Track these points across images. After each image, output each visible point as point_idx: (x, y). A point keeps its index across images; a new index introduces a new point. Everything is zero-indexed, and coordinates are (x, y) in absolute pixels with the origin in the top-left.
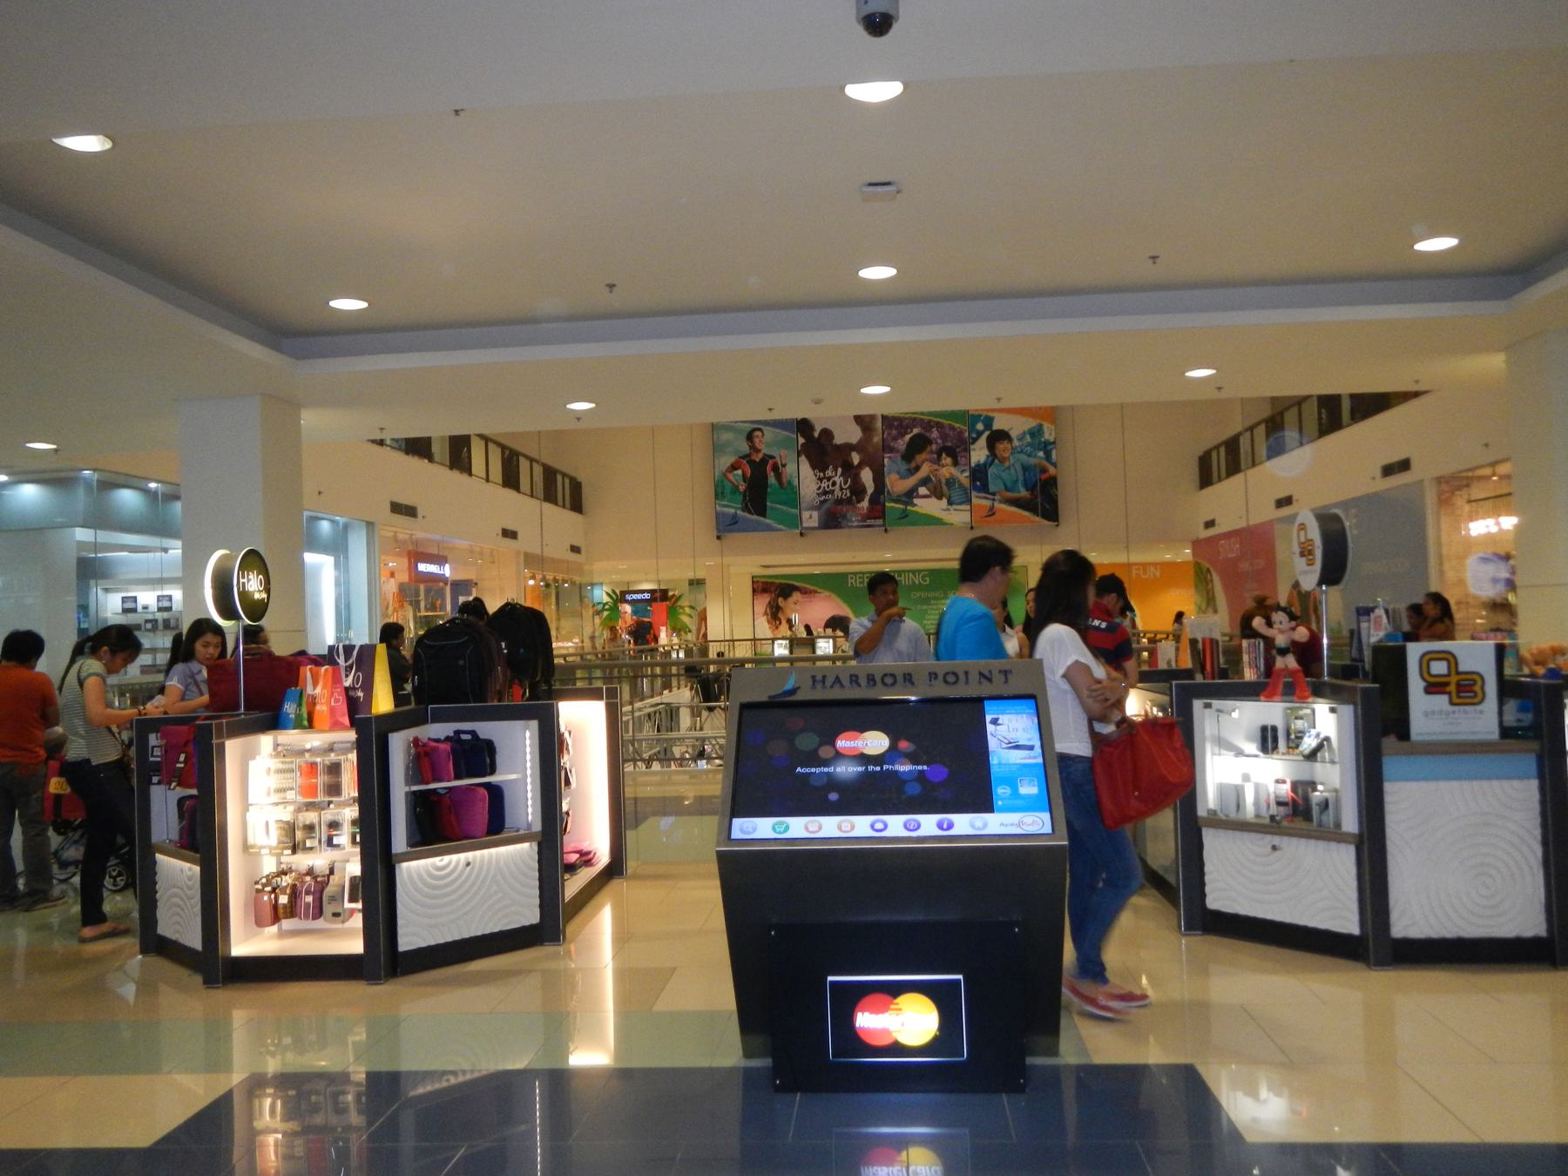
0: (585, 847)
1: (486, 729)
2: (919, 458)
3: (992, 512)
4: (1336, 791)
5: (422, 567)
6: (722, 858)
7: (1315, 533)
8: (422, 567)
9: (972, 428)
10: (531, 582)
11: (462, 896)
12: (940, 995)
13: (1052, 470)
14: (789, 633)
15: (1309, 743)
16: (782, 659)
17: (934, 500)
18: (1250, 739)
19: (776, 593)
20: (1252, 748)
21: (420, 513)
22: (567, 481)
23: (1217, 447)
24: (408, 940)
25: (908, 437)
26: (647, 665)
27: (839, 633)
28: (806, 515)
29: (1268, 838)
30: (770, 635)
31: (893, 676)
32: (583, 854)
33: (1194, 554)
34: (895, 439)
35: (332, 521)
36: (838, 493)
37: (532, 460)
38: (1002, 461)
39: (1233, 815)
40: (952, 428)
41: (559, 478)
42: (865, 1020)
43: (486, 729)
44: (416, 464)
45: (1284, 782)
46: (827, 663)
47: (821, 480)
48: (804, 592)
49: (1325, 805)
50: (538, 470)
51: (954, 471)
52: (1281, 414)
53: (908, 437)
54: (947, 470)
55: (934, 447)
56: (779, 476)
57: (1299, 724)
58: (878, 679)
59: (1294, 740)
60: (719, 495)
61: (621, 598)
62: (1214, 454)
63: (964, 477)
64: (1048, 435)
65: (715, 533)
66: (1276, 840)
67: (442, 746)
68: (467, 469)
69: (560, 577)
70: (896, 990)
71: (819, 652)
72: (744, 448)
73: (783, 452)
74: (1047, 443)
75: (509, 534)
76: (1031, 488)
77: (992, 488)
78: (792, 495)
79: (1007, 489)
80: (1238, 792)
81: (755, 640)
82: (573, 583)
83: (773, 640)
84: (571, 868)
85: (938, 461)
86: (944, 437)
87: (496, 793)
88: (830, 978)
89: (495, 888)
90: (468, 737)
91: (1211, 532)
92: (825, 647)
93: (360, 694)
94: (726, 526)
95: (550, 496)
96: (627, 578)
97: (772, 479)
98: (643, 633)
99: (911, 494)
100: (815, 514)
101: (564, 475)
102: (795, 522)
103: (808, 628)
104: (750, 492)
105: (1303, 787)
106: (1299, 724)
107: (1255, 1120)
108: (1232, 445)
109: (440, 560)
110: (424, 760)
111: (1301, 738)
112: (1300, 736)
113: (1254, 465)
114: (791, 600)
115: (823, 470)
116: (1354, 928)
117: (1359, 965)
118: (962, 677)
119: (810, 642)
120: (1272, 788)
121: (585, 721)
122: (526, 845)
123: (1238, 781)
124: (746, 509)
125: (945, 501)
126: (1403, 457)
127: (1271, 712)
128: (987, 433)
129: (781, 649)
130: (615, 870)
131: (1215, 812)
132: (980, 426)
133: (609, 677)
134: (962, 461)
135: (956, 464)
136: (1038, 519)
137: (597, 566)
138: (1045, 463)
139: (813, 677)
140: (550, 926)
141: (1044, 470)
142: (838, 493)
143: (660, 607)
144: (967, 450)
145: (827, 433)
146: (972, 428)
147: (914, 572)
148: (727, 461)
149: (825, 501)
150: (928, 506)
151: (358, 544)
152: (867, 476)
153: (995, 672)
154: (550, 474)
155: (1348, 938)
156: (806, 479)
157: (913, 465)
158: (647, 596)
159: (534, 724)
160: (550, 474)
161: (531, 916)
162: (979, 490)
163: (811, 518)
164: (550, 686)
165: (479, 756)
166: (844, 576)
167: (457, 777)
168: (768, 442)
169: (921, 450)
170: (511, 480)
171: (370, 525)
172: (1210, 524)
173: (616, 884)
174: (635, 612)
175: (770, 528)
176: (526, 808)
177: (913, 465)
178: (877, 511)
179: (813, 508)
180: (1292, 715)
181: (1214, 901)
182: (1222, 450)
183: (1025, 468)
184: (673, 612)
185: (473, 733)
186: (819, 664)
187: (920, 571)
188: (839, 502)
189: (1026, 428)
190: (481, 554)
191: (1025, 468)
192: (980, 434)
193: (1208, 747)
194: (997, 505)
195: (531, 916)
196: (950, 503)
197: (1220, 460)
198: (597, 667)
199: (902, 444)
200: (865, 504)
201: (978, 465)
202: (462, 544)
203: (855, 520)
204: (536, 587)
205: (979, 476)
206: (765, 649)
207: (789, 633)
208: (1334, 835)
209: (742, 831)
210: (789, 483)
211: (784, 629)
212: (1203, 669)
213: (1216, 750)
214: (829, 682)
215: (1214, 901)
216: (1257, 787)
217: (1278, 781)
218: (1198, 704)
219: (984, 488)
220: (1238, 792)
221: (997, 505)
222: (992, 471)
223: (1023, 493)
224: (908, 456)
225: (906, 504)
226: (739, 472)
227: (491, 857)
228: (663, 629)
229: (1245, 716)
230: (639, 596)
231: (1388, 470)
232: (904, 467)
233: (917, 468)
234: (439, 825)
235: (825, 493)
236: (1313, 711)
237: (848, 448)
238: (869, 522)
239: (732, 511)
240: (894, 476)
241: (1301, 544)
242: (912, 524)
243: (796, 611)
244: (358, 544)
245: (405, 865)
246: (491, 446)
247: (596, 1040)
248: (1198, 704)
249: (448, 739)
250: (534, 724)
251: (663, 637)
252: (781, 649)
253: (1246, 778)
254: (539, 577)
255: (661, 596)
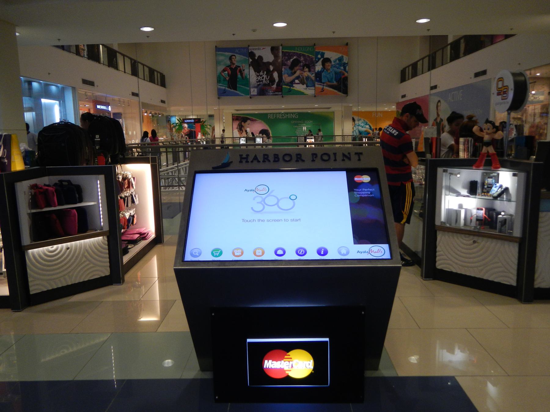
0: (143, 230)
1: (76, 179)
2: (296, 68)
3: (323, 90)
4: (511, 215)
5: (98, 107)
6: (178, 272)
7: (510, 82)
8: (98, 107)
9: (316, 57)
10: (146, 114)
11: (65, 264)
12: (311, 349)
13: (346, 74)
14: (246, 136)
15: (495, 191)
16: (243, 145)
17: (301, 85)
18: (464, 187)
19: (241, 120)
20: (465, 192)
21: (81, 81)
22: (159, 74)
23: (409, 66)
24: (35, 288)
25: (292, 60)
26: (190, 146)
27: (264, 136)
28: (252, 90)
29: (471, 237)
30: (239, 136)
31: (290, 155)
32: (141, 234)
33: (397, 108)
34: (287, 60)
35: (57, 86)
36: (264, 81)
37: (144, 65)
38: (327, 71)
39: (453, 225)
40: (309, 57)
41: (156, 73)
42: (269, 364)
43: (76, 179)
44: (65, 53)
45: (482, 209)
46: (260, 147)
47: (258, 76)
48: (252, 120)
49: (504, 222)
50: (147, 70)
51: (309, 74)
52: (435, 53)
53: (292, 60)
54: (306, 73)
55: (302, 64)
56: (242, 74)
57: (490, 181)
58: (281, 157)
59: (486, 189)
60: (219, 81)
61: (183, 121)
62: (407, 69)
63: (313, 76)
64: (345, 60)
65: (217, 96)
66: (476, 238)
67: (50, 188)
68: (116, 67)
69: (157, 112)
70: (288, 347)
71: (257, 142)
72: (228, 63)
73: (244, 65)
74: (345, 64)
75: (135, 94)
76: (338, 80)
77: (323, 81)
78: (246, 82)
79: (329, 81)
80: (458, 213)
81: (233, 138)
82: (163, 115)
83: (240, 138)
84: (134, 242)
85: (303, 70)
86: (305, 60)
87: (83, 213)
88: (249, 340)
89: (84, 259)
90: (66, 183)
91: (404, 99)
92: (259, 141)
93: (6, 161)
94: (221, 94)
95: (152, 80)
96: (185, 114)
97: (239, 76)
98: (192, 135)
99: (292, 83)
100: (256, 90)
101: (157, 72)
102: (248, 93)
103: (252, 133)
104: (231, 82)
105: (491, 212)
106: (490, 181)
107: (450, 362)
108: (414, 66)
109: (107, 104)
110: (39, 197)
111: (491, 188)
112: (490, 187)
113: (422, 73)
114: (247, 123)
115: (259, 72)
116: (514, 283)
117: (513, 300)
118: (332, 157)
119: (254, 140)
120: (475, 212)
121: (139, 172)
122: (101, 238)
123: (456, 207)
124: (229, 87)
125: (305, 85)
126: (484, 69)
127: (476, 174)
128: (322, 59)
129: (243, 141)
130: (158, 240)
131: (444, 223)
132: (319, 56)
133: (149, 152)
134: (312, 70)
135: (310, 71)
136: (340, 93)
137: (172, 108)
138: (344, 72)
139: (241, 156)
140: (116, 275)
141: (343, 74)
142: (264, 81)
143: (198, 125)
144: (314, 66)
145: (260, 58)
146: (316, 57)
147: (292, 113)
148: (221, 68)
149: (259, 84)
150: (299, 87)
151: (69, 97)
152: (276, 75)
153: (353, 154)
154: (152, 71)
155: (510, 286)
156: (252, 76)
157: (293, 71)
158: (192, 121)
159: (102, 177)
160: (152, 71)
161: (106, 272)
162: (317, 81)
163: (254, 91)
164: (124, 156)
165: (75, 193)
166: (266, 115)
167: (60, 204)
168: (238, 59)
169: (296, 65)
170: (135, 73)
171: (74, 89)
172: (404, 96)
173: (158, 247)
174: (189, 127)
175: (237, 95)
176: (102, 220)
177: (293, 71)
178: (279, 89)
179: (255, 87)
180: (485, 176)
181: (440, 265)
182: (410, 68)
183: (336, 73)
184: (203, 126)
185: (69, 182)
186: (257, 147)
187: (295, 113)
188: (265, 85)
189: (337, 57)
190: (124, 102)
191: (336, 73)
192: (319, 59)
193: (443, 191)
194: (325, 87)
195: (106, 272)
196: (307, 86)
197: (410, 71)
198: (181, 147)
199: (289, 62)
200: (275, 86)
201: (318, 72)
202: (116, 98)
203: (271, 92)
204: (148, 116)
205: (318, 75)
206: (237, 141)
207: (246, 136)
208: (510, 239)
209: (192, 255)
210: (246, 77)
211: (244, 134)
212: (431, 152)
213: (448, 193)
214: (250, 159)
215: (440, 265)
216: (466, 210)
217: (478, 209)
218: (440, 170)
219: (320, 81)
220: (458, 213)
221: (325, 87)
222: (323, 74)
223: (335, 83)
224: (292, 67)
225: (290, 86)
226: (226, 72)
227: (76, 246)
228: (199, 133)
229: (465, 175)
230: (190, 121)
231: (477, 75)
232: (290, 72)
233: (295, 72)
234: (49, 229)
235: (260, 81)
236: (498, 174)
237: (269, 63)
238: (276, 93)
239: (224, 88)
240: (286, 75)
241: (498, 88)
242: (293, 94)
243: (248, 127)
244: (69, 97)
245: (30, 251)
246: (145, 67)
247: (151, 311)
248: (440, 170)
249: (55, 185)
250: (102, 177)
251: (199, 136)
252: (243, 141)
253: (461, 206)
254: (149, 112)
255: (197, 121)
